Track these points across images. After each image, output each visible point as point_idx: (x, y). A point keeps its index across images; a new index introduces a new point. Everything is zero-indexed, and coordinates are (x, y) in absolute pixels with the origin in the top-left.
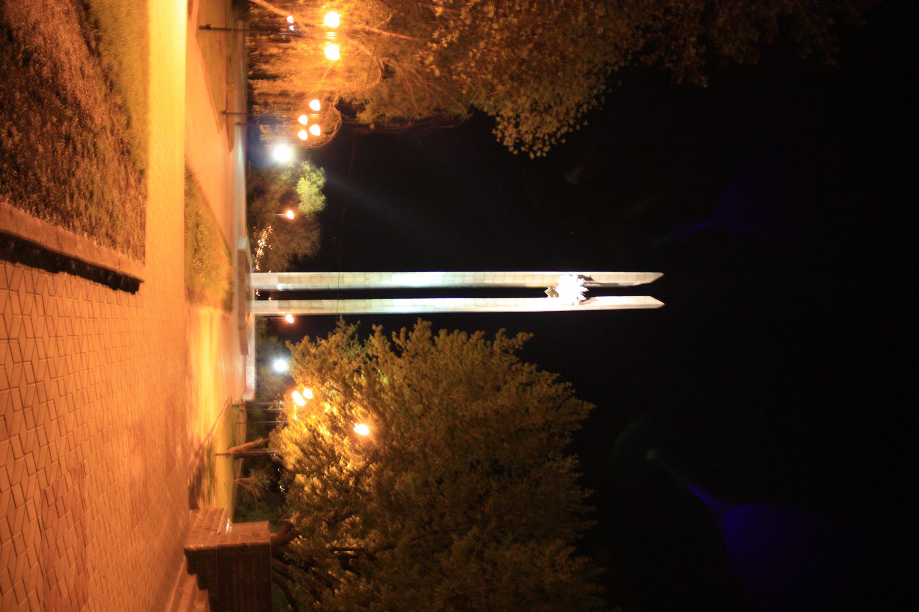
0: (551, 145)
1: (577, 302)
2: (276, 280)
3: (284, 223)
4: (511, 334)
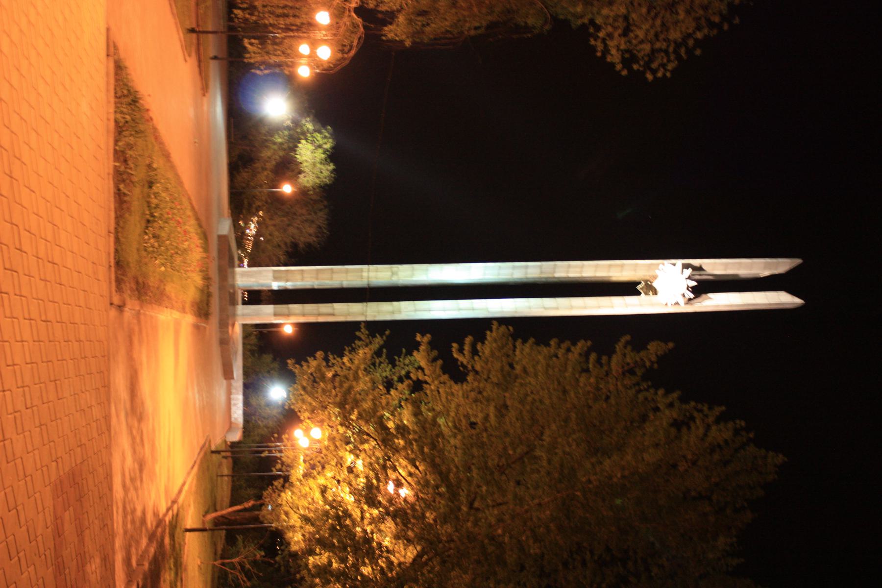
0: (679, 57)
1: (682, 301)
2: (271, 276)
3: (278, 200)
4: (638, 345)
